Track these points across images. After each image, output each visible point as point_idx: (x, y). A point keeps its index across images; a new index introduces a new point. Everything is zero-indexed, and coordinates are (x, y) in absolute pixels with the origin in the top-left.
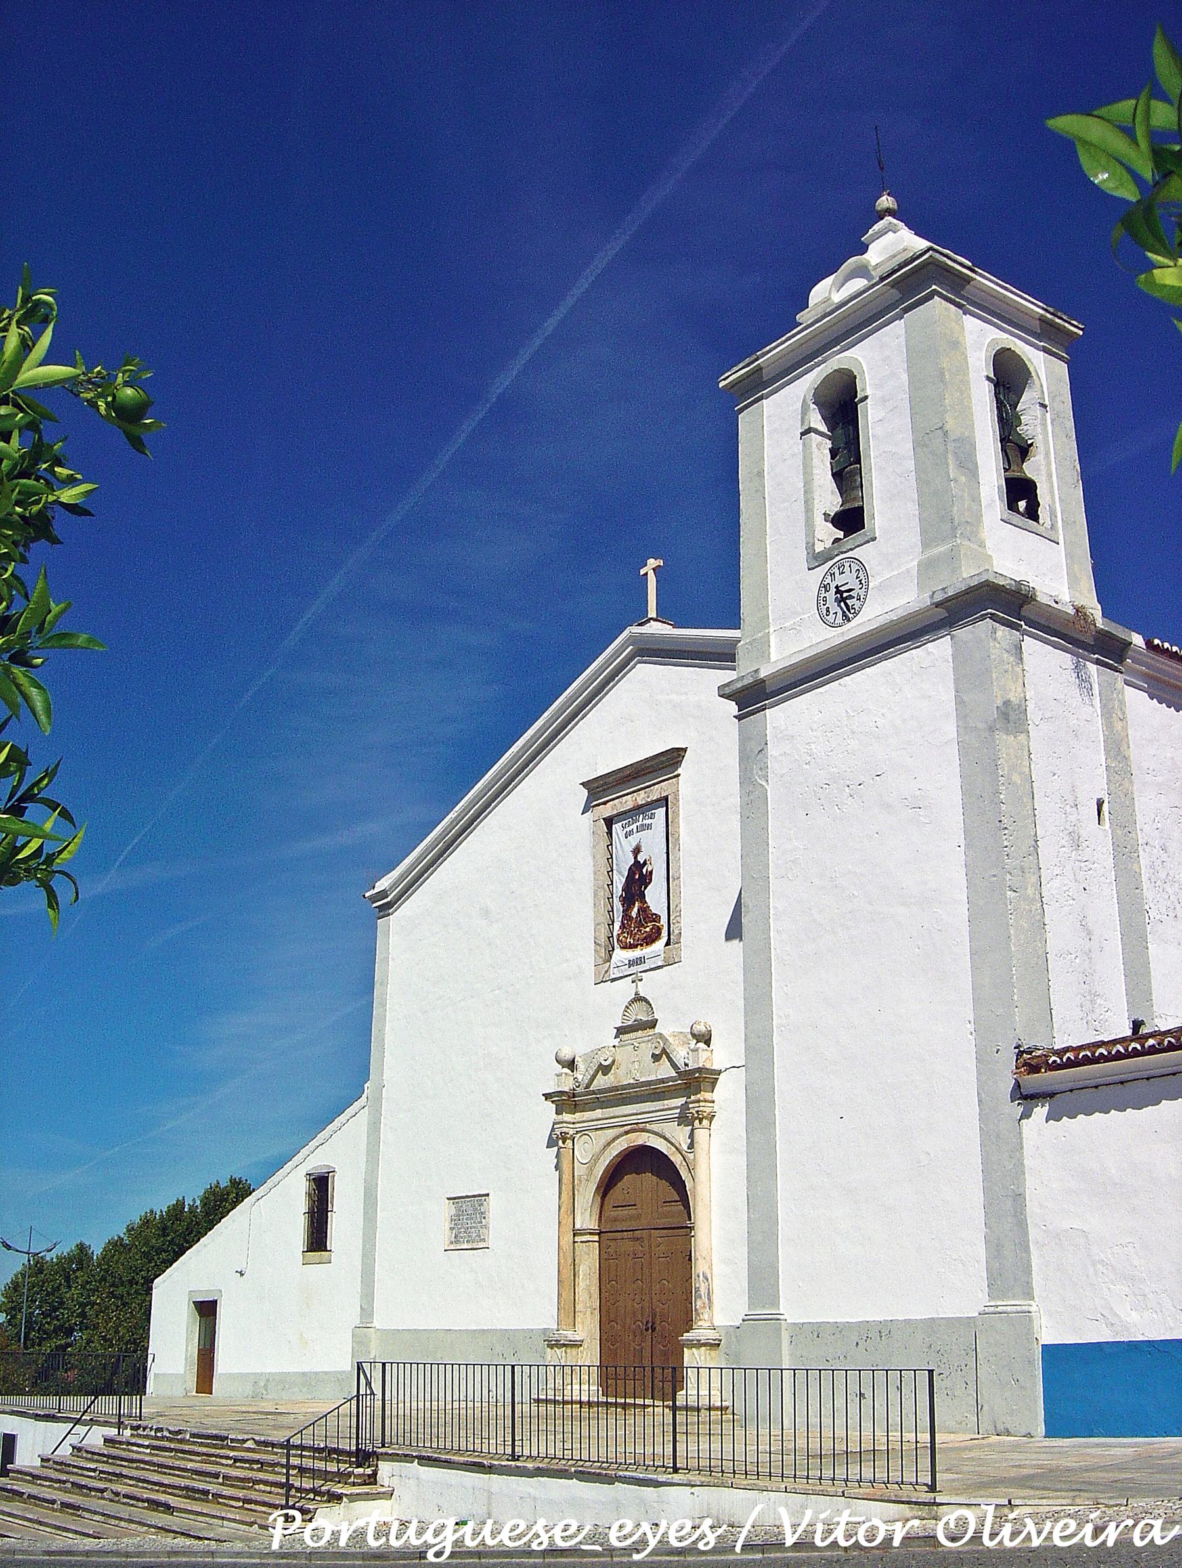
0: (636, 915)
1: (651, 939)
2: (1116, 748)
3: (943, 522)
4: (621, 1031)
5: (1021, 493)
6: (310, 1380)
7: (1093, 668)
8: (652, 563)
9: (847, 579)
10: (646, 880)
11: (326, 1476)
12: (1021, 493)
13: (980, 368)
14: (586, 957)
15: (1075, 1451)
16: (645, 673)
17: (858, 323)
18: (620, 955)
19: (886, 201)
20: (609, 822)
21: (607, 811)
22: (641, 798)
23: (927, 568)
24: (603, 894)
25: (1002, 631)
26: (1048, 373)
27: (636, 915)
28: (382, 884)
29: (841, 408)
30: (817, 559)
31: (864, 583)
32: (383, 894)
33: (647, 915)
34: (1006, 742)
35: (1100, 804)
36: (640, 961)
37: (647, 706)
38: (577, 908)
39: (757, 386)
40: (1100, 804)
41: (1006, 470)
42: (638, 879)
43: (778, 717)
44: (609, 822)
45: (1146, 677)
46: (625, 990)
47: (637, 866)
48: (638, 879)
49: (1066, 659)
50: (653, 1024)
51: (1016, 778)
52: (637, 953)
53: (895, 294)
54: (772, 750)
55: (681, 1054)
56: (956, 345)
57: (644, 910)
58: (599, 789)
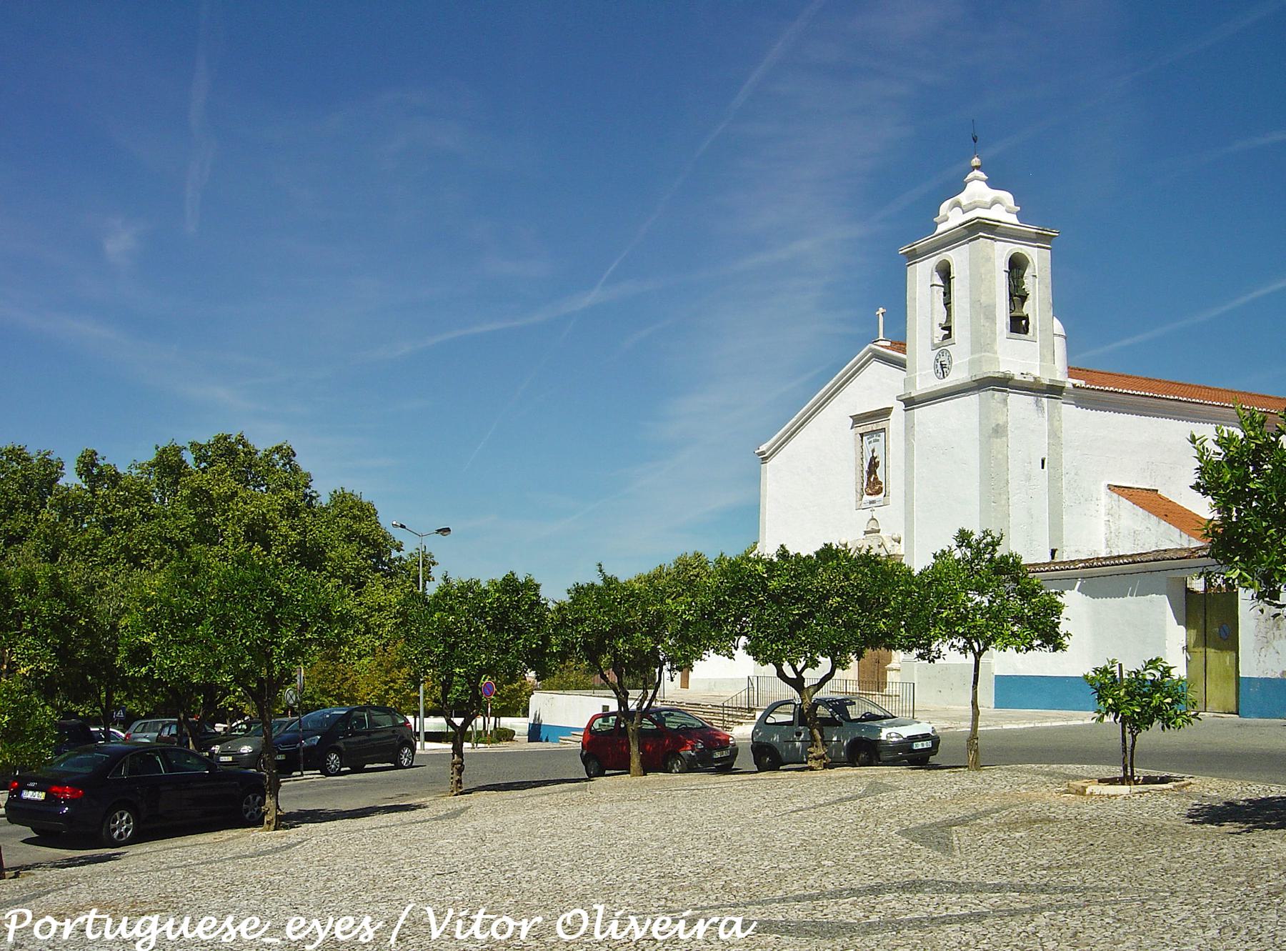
0: (873, 483)
1: (878, 492)
2: (1054, 435)
3: (981, 344)
4: (866, 533)
5: (1019, 325)
6: (734, 682)
7: (1045, 400)
8: (881, 310)
9: (944, 359)
10: (877, 465)
11: (737, 717)
12: (1019, 325)
13: (1002, 265)
14: (853, 497)
15: (999, 711)
16: (876, 366)
17: (953, 240)
18: (867, 498)
19: (976, 161)
20: (862, 435)
21: (861, 430)
22: (874, 427)
23: (972, 363)
24: (859, 468)
25: (997, 394)
26: (1038, 258)
27: (873, 483)
28: (763, 448)
29: (945, 273)
30: (935, 347)
31: (950, 362)
32: (763, 453)
33: (877, 482)
34: (997, 442)
35: (1043, 461)
36: (873, 502)
37: (875, 386)
38: (849, 477)
39: (914, 256)
40: (1043, 461)
41: (1011, 311)
42: (873, 465)
43: (919, 413)
44: (862, 435)
45: (1074, 399)
46: (867, 514)
47: (873, 458)
48: (873, 465)
49: (1031, 399)
50: (878, 531)
51: (1000, 456)
52: (872, 498)
53: (966, 232)
54: (916, 428)
55: (888, 545)
56: (989, 259)
57: (876, 479)
58: (858, 419)
